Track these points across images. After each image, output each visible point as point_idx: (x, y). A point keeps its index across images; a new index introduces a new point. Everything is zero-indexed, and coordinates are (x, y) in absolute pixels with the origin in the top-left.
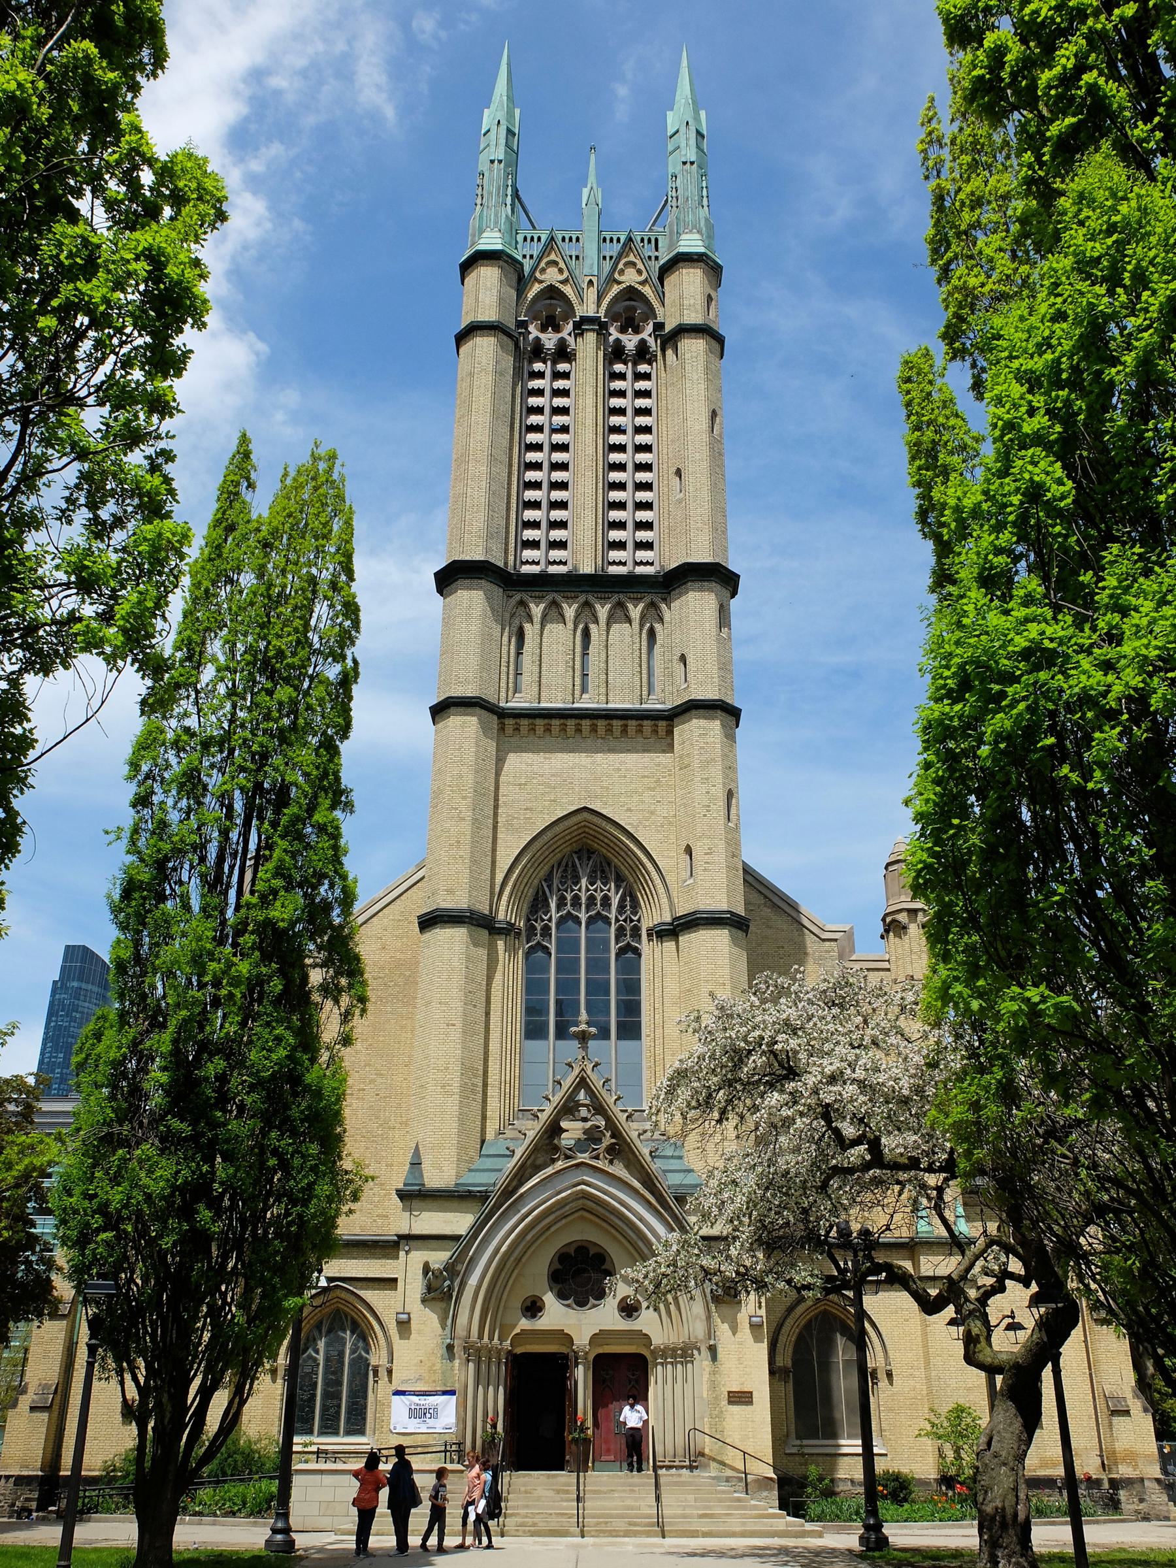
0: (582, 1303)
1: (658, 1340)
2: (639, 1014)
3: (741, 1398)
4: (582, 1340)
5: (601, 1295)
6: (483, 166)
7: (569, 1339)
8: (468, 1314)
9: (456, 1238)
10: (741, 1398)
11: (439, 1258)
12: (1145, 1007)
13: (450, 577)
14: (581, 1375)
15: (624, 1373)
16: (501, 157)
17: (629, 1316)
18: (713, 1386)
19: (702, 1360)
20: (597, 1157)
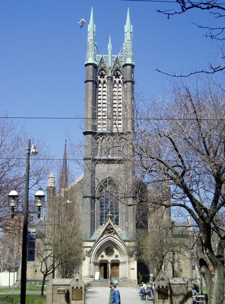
0: (109, 255)
1: (121, 261)
2: (118, 221)
3: (133, 269)
4: (110, 261)
5: (112, 254)
6: (88, 41)
7: (108, 261)
8: (93, 257)
9: (91, 247)
10: (133, 269)
11: (89, 249)
12: (88, 98)
13: (85, 133)
14: (109, 265)
15: (116, 264)
16: (92, 39)
17: (117, 257)
18: (129, 267)
19: (127, 264)
20: (112, 235)
